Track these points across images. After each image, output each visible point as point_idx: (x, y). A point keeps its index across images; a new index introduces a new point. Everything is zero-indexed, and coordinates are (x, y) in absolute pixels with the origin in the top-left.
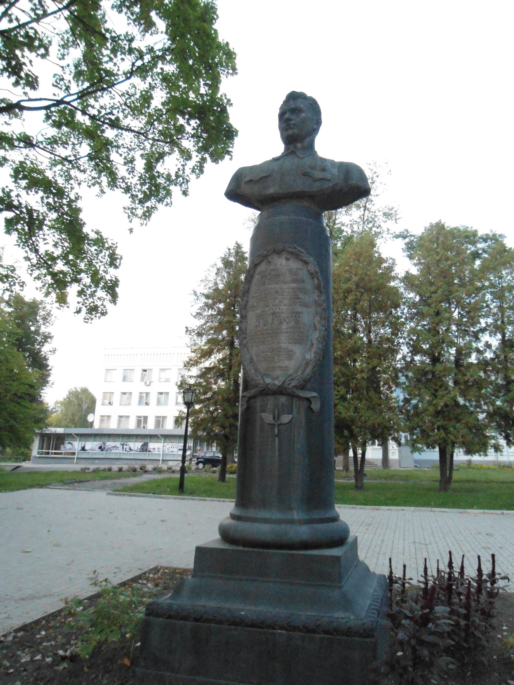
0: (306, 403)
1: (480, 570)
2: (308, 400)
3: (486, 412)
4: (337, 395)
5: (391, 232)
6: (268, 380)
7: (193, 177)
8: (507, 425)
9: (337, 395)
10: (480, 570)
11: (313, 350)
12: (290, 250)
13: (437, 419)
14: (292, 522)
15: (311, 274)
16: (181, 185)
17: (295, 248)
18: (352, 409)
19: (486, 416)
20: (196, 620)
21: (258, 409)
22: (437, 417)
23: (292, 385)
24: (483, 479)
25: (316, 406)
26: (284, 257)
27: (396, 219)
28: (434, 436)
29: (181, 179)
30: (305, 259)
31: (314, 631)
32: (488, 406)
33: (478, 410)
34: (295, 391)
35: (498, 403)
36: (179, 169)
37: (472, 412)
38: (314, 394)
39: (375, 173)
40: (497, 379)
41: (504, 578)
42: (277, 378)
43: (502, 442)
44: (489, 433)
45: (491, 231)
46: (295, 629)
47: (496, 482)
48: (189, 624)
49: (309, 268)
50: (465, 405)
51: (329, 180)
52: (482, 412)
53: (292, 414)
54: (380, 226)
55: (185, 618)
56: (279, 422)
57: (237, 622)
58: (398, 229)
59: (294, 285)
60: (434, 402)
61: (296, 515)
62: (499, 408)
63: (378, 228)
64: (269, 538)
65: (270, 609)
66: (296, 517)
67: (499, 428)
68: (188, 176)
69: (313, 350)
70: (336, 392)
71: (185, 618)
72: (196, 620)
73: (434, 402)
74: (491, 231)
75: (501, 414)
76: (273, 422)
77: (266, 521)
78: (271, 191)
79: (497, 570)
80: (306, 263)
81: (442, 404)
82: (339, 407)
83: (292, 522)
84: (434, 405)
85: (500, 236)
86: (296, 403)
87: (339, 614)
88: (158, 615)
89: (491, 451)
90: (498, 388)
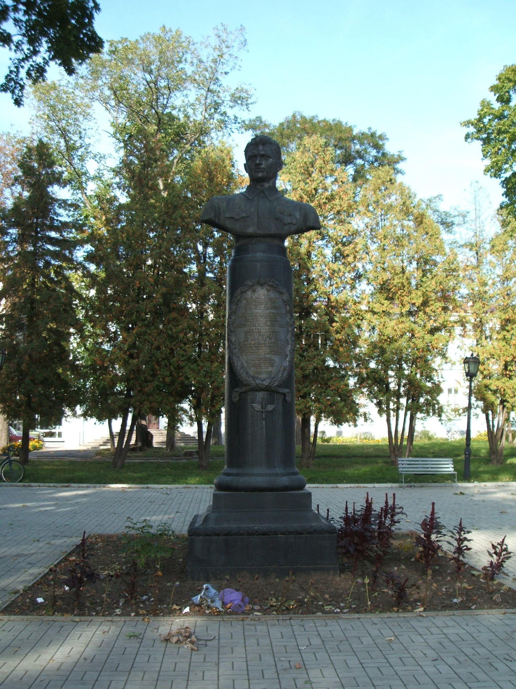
1: (386, 502)
2: (284, 395)
4: (183, 356)
5: (239, 120)
6: (258, 382)
7: (28, 83)
9: (183, 356)
10: (386, 502)
11: (287, 359)
12: (270, 283)
14: (277, 475)
15: (285, 302)
16: (13, 92)
17: (274, 282)
20: (226, 535)
21: (249, 401)
25: (288, 398)
26: (265, 288)
27: (247, 105)
28: (299, 405)
29: (13, 83)
30: (281, 290)
31: (301, 533)
36: (11, 72)
38: (288, 390)
39: (224, 42)
41: (400, 508)
42: (265, 380)
45: (370, 129)
46: (290, 533)
47: (360, 457)
48: (221, 537)
49: (284, 298)
50: (335, 367)
54: (225, 113)
55: (218, 535)
57: (252, 533)
58: (245, 115)
59: (273, 311)
61: (279, 471)
62: (374, 371)
63: (222, 115)
64: (264, 485)
65: (271, 525)
66: (279, 472)
68: (22, 79)
70: (182, 352)
71: (218, 535)
72: (226, 535)
73: (302, 364)
74: (370, 129)
77: (258, 475)
78: (250, 230)
79: (396, 503)
80: (281, 293)
81: (311, 367)
82: (186, 369)
83: (277, 475)
84: (302, 368)
85: (381, 137)
87: (314, 524)
88: (198, 535)
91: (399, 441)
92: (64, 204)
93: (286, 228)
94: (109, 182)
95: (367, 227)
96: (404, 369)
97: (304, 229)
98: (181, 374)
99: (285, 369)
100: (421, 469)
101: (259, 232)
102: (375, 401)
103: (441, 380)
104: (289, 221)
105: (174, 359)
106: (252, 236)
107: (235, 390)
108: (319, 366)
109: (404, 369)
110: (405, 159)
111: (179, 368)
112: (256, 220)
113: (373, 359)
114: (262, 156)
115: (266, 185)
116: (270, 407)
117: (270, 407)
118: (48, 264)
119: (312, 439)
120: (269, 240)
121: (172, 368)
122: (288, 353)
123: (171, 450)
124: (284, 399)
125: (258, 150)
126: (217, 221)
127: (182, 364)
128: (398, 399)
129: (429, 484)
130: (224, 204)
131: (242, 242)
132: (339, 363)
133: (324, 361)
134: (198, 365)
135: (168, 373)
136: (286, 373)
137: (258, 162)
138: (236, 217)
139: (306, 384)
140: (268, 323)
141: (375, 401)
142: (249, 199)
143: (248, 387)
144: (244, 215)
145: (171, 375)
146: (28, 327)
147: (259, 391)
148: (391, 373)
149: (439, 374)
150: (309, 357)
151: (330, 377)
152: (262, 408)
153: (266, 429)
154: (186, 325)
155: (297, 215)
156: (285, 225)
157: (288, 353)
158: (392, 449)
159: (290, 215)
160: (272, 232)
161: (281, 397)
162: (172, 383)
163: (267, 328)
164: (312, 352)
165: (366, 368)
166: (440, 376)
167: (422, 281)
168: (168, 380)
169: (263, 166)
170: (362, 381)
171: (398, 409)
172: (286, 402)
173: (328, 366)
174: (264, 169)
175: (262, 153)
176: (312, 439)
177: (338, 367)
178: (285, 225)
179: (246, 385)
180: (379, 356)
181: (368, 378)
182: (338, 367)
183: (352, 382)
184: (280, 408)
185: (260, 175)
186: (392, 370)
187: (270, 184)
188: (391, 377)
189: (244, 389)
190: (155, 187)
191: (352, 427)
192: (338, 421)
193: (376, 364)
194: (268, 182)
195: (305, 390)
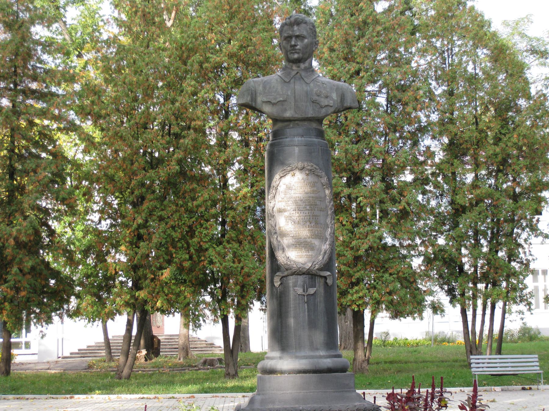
0: (322, 280)
2: (325, 278)
3: (424, 255)
8: (451, 274)
11: (328, 243)
13: (355, 269)
18: (230, 256)
19: (423, 261)
22: (355, 266)
23: (316, 268)
24: (412, 359)
25: (329, 282)
30: (319, 174)
32: (426, 247)
33: (412, 252)
34: (318, 272)
35: (441, 241)
37: (405, 257)
38: (329, 273)
40: (428, 116)
43: (443, 298)
44: (422, 286)
49: (323, 181)
50: (394, 246)
51: (331, 106)
52: (419, 255)
53: (315, 287)
56: (308, 293)
60: (354, 243)
61: (322, 353)
62: (442, 250)
67: (443, 280)
69: (328, 243)
73: (354, 243)
75: (444, 259)
76: (304, 293)
78: (288, 114)
82: (211, 252)
86: (318, 280)
89: (428, 313)
90: (440, 219)
91: (477, 338)
92: (48, 46)
93: (324, 110)
94: (95, 7)
95: (430, 67)
96: (482, 246)
97: (342, 109)
98: (203, 258)
99: (325, 253)
100: (499, 369)
101: (296, 116)
102: (446, 287)
103: (530, 258)
104: (326, 104)
105: (195, 240)
106: (289, 120)
107: (277, 274)
108: (375, 245)
109: (482, 246)
110: (114, 320)
111: (201, 250)
112: (293, 104)
113: (442, 233)
114: (297, 37)
115: (302, 66)
116: (312, 291)
117: (312, 291)
118: (31, 124)
119: (366, 337)
120: (306, 123)
121: (192, 250)
122: (328, 237)
123: (185, 358)
124: (326, 283)
125: (293, 31)
126: (254, 105)
127: (205, 246)
128: (475, 284)
129: (510, 387)
130: (261, 88)
131: (280, 125)
132: (399, 239)
133: (381, 238)
134: (225, 248)
135: (187, 256)
136: (326, 257)
137: (293, 43)
138: (273, 101)
139: (359, 267)
140: (308, 208)
141: (446, 287)
142: (285, 82)
143: (289, 272)
144: (281, 99)
145: (191, 258)
146: (473, 298)
147: (301, 275)
148: (464, 251)
149: (527, 250)
150: (361, 233)
151: (387, 258)
152: (304, 291)
153: (308, 312)
154: (208, 196)
155: (334, 96)
156: (322, 107)
157: (328, 237)
158: (469, 348)
159: (327, 97)
160: (310, 116)
161: (322, 280)
162: (191, 270)
163: (307, 212)
164: (362, 229)
165: (433, 245)
166: (527, 254)
167: (501, 133)
168: (187, 264)
169: (298, 47)
170: (428, 261)
171: (475, 297)
172: (328, 285)
173: (386, 244)
174: (300, 50)
175: (298, 34)
176: (366, 337)
177: (397, 245)
178: (322, 107)
179: (287, 270)
180: (449, 230)
181: (435, 259)
182: (397, 245)
183: (417, 262)
184: (322, 290)
185: (296, 56)
186: (466, 248)
187: (307, 64)
188: (465, 256)
189: (286, 273)
190: (162, 25)
191: (418, 320)
192: (397, 314)
193: (446, 239)
194: (304, 62)
195: (357, 275)
